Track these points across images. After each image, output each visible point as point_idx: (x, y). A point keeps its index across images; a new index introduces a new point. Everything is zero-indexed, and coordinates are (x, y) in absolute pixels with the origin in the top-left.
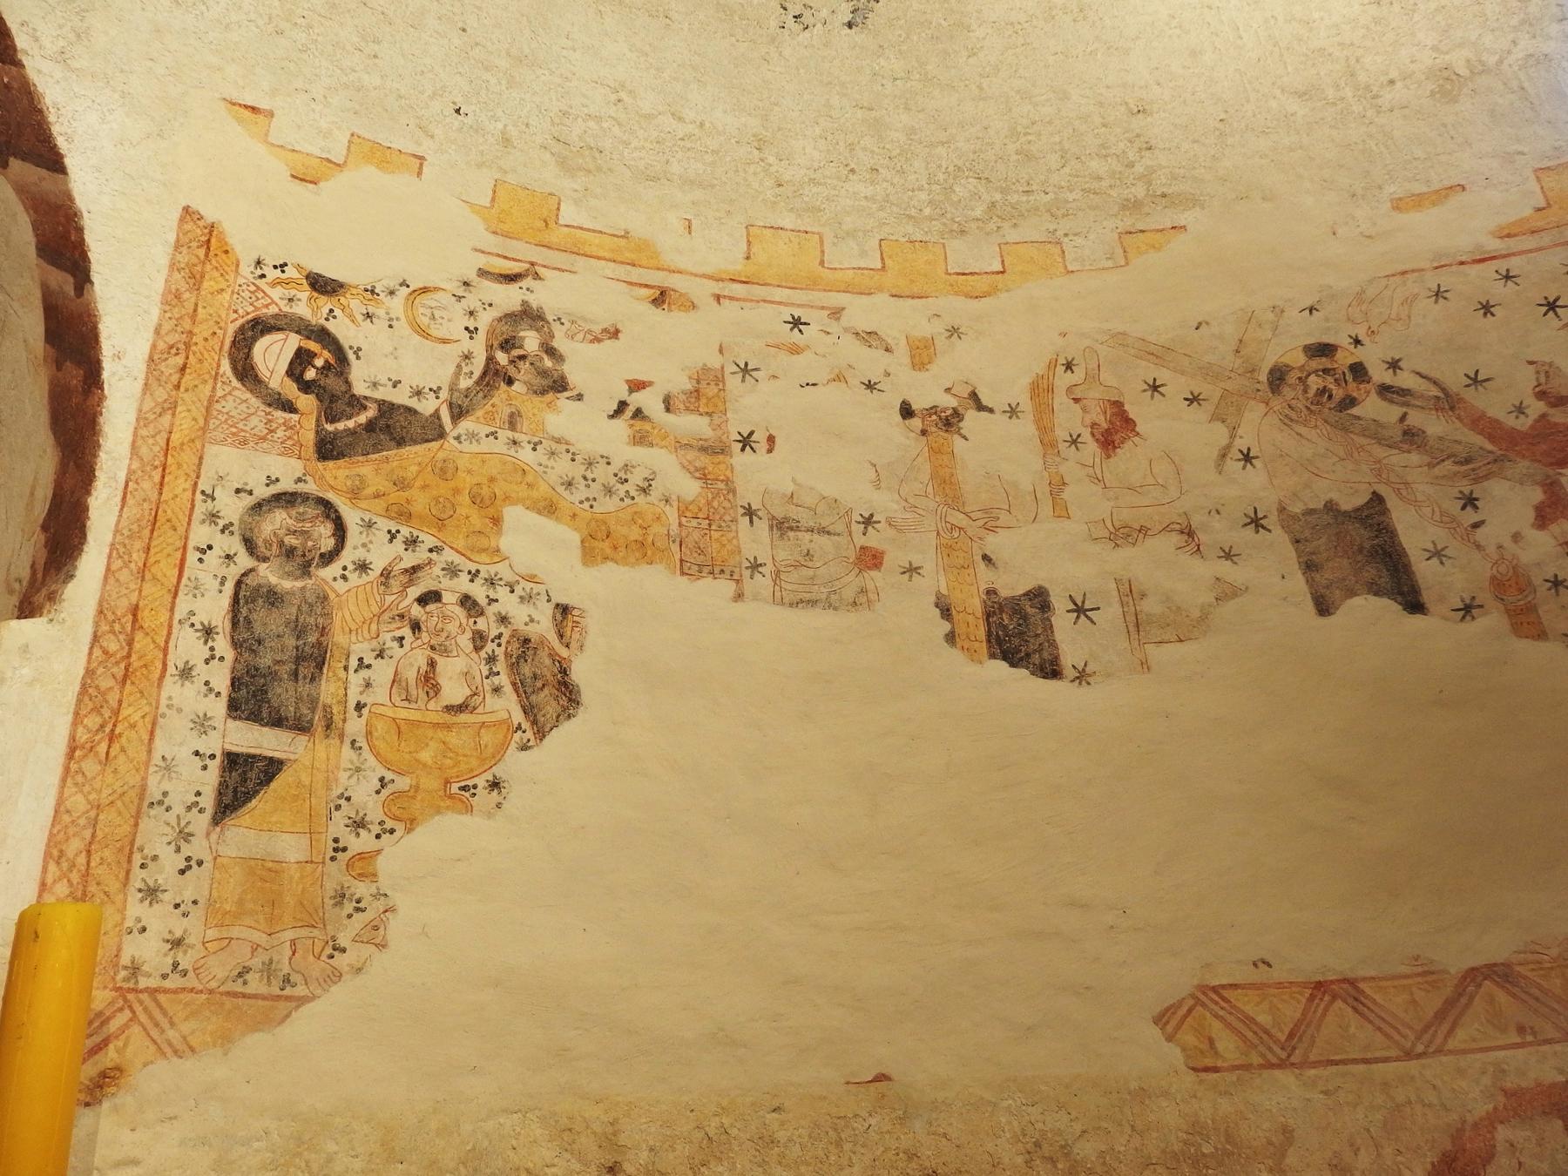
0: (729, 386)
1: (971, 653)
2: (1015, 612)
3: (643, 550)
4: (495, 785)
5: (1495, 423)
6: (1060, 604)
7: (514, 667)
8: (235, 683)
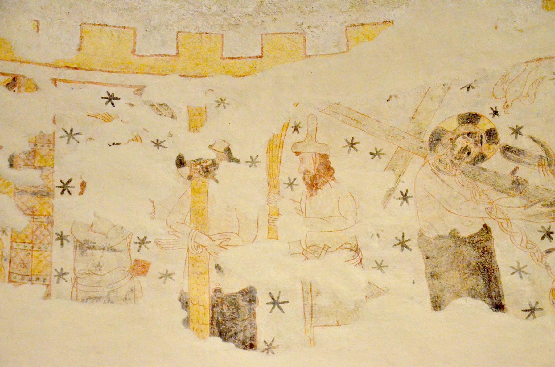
0: (57, 147)
1: (198, 332)
2: (231, 304)
6: (262, 298)
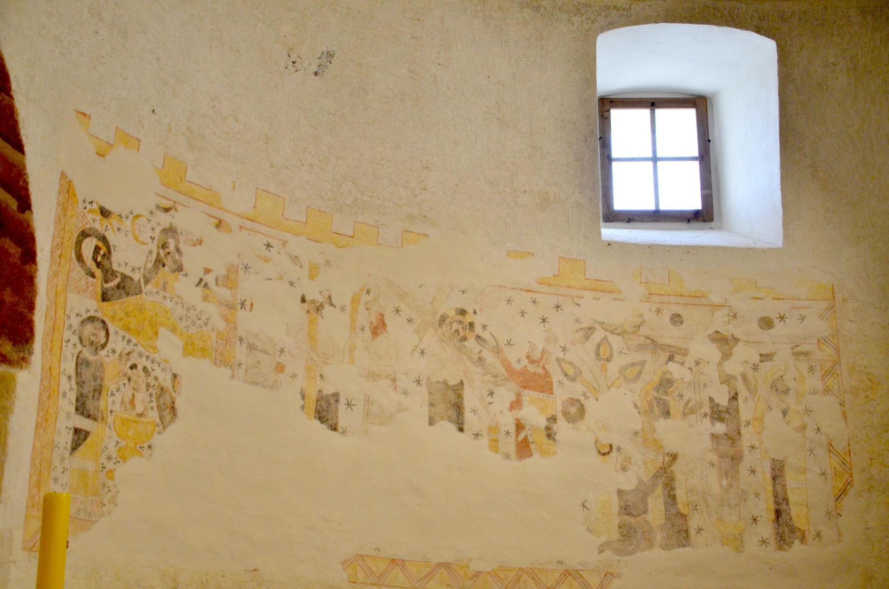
3: (203, 352)
4: (150, 447)
5: (509, 364)
6: (343, 401)
7: (158, 399)
8: (77, 400)
